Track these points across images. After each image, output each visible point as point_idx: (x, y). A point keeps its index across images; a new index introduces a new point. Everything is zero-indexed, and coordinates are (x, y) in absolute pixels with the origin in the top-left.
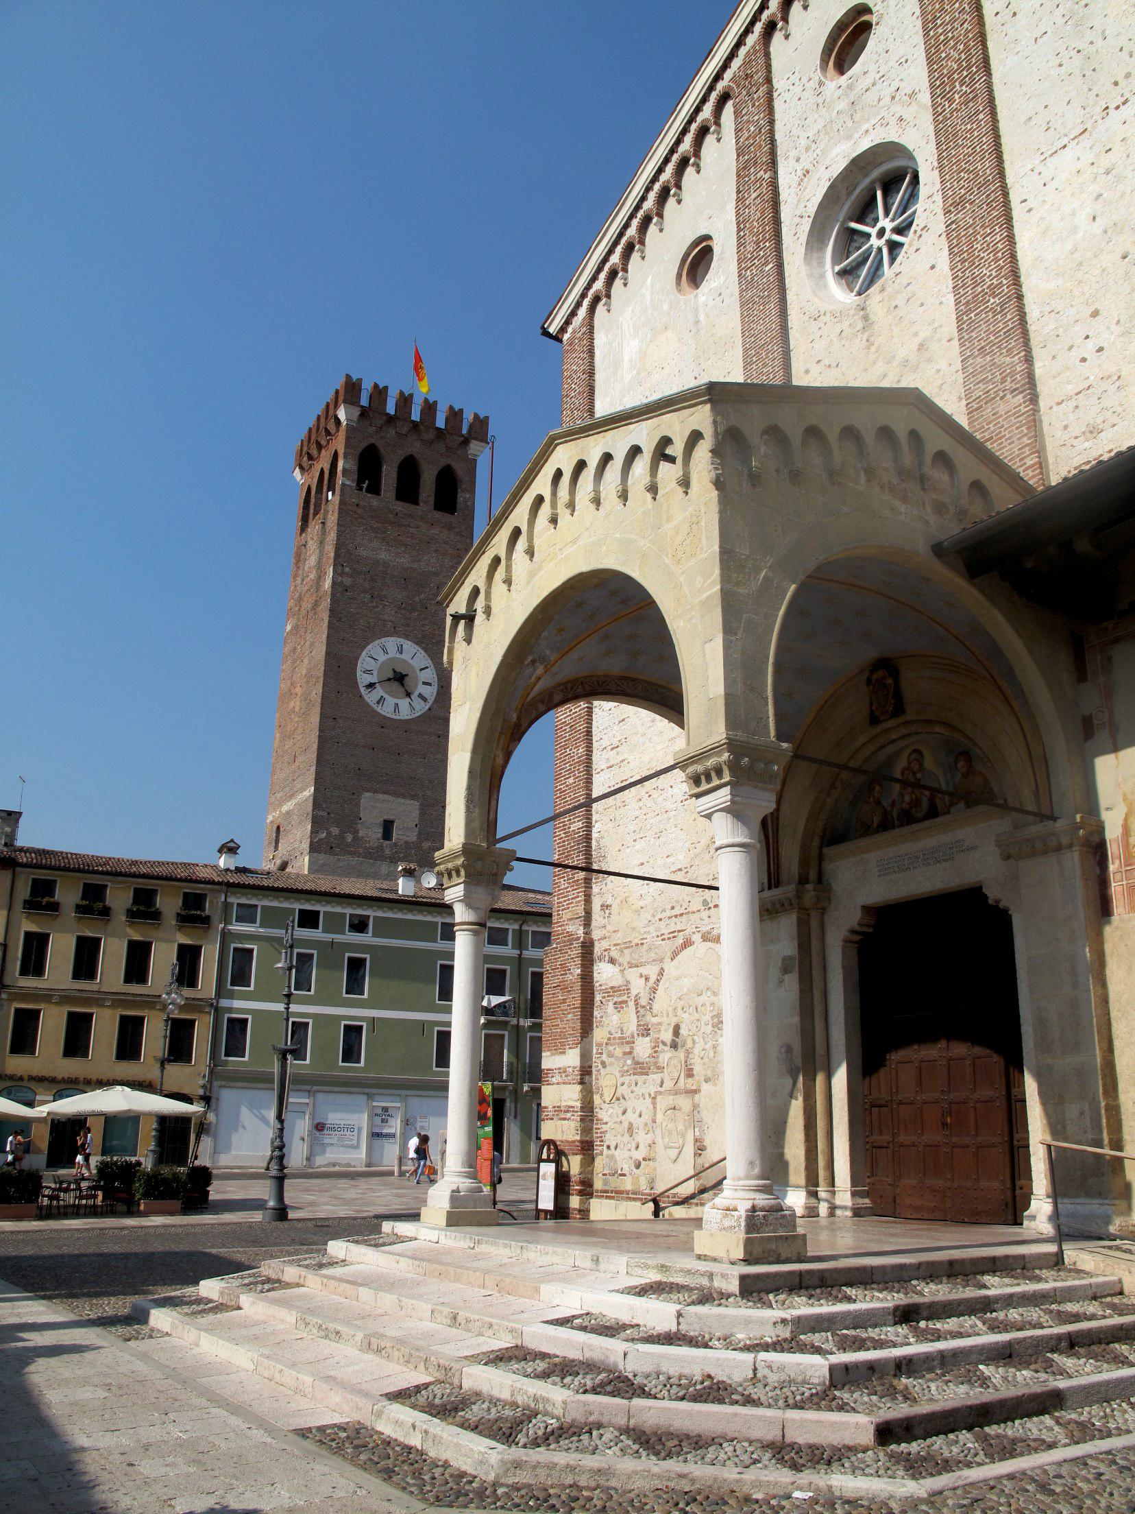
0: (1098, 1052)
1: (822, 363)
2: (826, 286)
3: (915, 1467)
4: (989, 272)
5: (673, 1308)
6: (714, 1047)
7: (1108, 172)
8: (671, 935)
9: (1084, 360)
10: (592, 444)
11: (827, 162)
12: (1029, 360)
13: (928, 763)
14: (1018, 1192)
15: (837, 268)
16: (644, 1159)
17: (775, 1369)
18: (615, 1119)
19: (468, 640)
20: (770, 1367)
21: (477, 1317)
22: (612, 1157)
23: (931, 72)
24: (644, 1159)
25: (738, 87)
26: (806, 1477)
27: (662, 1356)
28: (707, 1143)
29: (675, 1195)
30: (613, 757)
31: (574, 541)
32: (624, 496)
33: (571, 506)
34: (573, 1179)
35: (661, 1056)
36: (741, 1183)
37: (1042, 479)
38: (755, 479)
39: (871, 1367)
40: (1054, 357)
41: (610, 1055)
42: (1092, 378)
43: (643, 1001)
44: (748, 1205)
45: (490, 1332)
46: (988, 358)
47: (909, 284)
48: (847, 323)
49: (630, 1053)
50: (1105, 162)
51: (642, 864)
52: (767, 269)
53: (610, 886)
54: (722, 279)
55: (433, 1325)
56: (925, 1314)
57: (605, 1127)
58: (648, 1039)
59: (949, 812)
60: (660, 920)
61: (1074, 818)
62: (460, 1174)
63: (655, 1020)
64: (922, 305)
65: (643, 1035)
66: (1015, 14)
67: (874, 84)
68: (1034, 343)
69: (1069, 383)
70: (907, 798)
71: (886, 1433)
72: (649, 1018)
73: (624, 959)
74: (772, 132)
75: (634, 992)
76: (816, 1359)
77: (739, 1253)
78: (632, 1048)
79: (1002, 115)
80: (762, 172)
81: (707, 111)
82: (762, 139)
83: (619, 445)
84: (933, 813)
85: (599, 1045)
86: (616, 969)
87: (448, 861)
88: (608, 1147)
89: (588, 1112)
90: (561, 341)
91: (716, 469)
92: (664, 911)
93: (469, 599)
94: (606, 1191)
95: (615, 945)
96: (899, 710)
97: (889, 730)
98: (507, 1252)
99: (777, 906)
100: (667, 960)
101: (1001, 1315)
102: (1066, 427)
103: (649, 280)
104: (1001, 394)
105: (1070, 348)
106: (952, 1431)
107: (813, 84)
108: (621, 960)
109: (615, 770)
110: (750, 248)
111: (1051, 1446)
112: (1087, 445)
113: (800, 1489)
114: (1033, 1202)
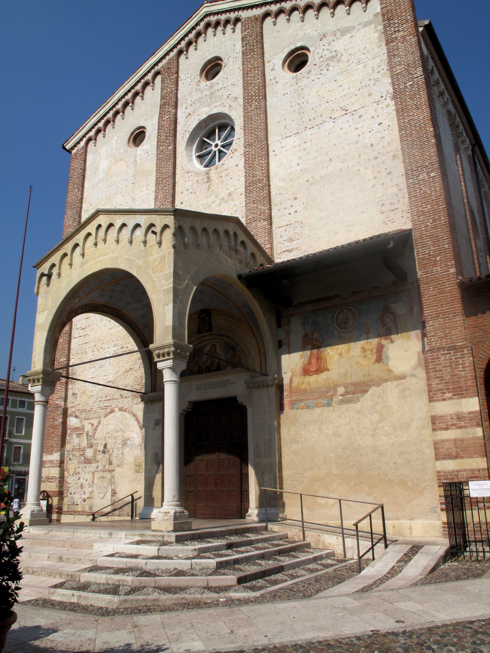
0: (277, 458)
1: (189, 191)
2: (192, 161)
3: (253, 589)
4: (259, 174)
5: (157, 548)
6: (122, 453)
7: (305, 150)
8: (105, 408)
9: (290, 214)
10: (117, 218)
11: (199, 113)
12: (270, 209)
13: (218, 350)
14: (243, 507)
15: (197, 154)
16: (88, 498)
17: (198, 564)
18: (74, 482)
19: (48, 285)
20: (197, 564)
21: (73, 557)
22: (72, 498)
23: (244, 93)
24: (88, 498)
25: (164, 71)
26: (222, 594)
27: (159, 563)
28: (117, 491)
29: (101, 512)
30: (82, 333)
31: (105, 255)
32: (131, 242)
33: (105, 240)
34: (54, 507)
35: (98, 456)
36: (171, 503)
37: (271, 253)
38: (185, 245)
39: (227, 562)
40: (279, 210)
41: (73, 455)
42: (292, 221)
43: (91, 434)
44: (174, 511)
45: (80, 562)
46: (256, 205)
47: (227, 169)
48: (201, 178)
49: (83, 455)
50: (304, 146)
51: (93, 378)
52: (170, 148)
53: (77, 385)
54: (149, 147)
55: (49, 562)
56: (235, 546)
57: (69, 485)
58: (92, 449)
59: (225, 369)
60: (100, 401)
61: (275, 376)
62: (34, 504)
63: (95, 442)
64: (231, 179)
65: (90, 448)
66: (277, 82)
67: (221, 89)
68: (272, 203)
69: (284, 221)
70: (209, 362)
71: (241, 581)
72: (93, 441)
73: (83, 415)
74: (177, 94)
75: (86, 430)
76: (211, 560)
77: (172, 528)
78: (84, 453)
79: (269, 117)
80: (171, 109)
81: (149, 77)
82: (172, 95)
83: (130, 222)
84: (219, 369)
85: (68, 451)
86: (78, 420)
87: (34, 375)
88: (71, 493)
89: (62, 479)
90: (71, 153)
91: (174, 241)
92: (102, 397)
93: (50, 267)
94: (69, 512)
95: (78, 410)
96: (210, 329)
97: (204, 336)
98: (66, 534)
99: (155, 399)
100: (103, 417)
101: (256, 545)
102: (281, 236)
103: (115, 138)
104: (259, 220)
105: (286, 208)
106: (256, 579)
107: (196, 80)
108: (80, 417)
109: (82, 338)
110: (163, 138)
111: (286, 581)
112: (288, 244)
113: (221, 598)
114: (249, 510)
